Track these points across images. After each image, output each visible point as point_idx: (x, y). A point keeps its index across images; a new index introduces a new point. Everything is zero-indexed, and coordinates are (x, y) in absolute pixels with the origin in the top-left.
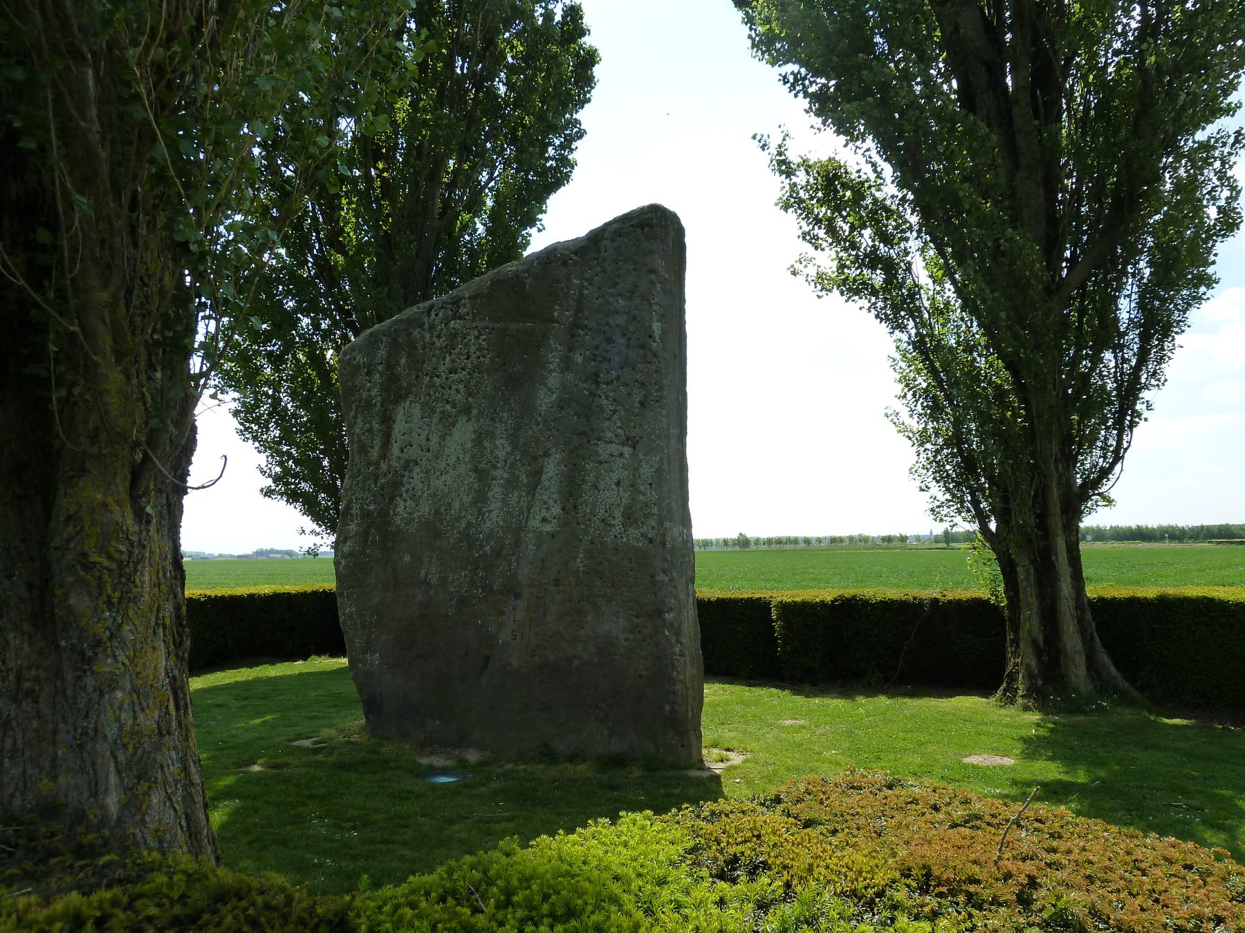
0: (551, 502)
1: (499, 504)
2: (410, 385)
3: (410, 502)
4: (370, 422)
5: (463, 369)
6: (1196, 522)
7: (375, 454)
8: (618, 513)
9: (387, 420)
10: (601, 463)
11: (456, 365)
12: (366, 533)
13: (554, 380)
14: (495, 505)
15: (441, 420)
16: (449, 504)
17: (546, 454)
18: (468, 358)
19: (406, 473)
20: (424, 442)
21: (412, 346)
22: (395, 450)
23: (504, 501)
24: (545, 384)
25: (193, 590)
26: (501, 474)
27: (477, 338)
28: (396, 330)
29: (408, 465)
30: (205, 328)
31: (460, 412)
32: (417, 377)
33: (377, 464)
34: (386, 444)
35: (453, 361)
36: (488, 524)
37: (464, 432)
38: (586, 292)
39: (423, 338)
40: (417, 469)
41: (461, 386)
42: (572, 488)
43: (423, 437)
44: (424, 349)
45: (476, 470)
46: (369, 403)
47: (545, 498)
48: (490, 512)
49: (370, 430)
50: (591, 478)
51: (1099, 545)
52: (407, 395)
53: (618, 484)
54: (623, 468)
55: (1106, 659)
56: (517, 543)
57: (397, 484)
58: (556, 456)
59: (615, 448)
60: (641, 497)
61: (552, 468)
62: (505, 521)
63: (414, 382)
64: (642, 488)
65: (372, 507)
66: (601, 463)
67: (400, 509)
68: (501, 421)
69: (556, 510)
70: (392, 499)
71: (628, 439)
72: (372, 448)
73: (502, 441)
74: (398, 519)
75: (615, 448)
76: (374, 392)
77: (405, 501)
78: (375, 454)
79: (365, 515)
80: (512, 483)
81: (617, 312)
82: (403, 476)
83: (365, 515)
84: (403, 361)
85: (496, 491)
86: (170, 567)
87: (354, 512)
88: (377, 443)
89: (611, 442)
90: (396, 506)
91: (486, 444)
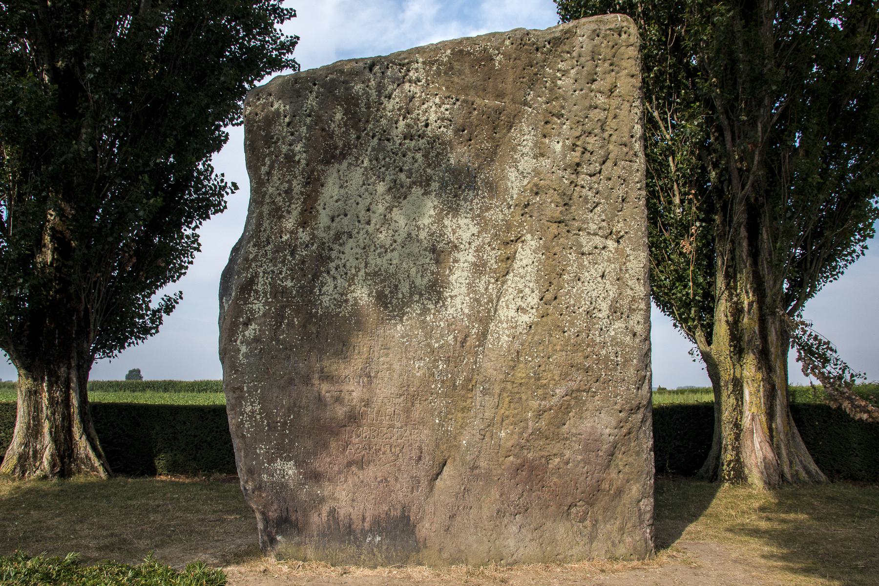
1: (464, 289)
2: (347, 145)
3: (340, 281)
8: (605, 306)
9: (314, 183)
10: (583, 254)
11: (413, 131)
12: (279, 316)
13: (527, 164)
15: (390, 189)
16: (396, 286)
19: (336, 247)
22: (324, 219)
23: (470, 286)
24: (516, 167)
28: (332, 80)
30: (797, 134)
31: (414, 183)
36: (451, 311)
38: (559, 82)
40: (351, 243)
41: (419, 156)
42: (551, 279)
43: (362, 207)
44: (368, 108)
46: (290, 158)
49: (289, 192)
50: (573, 268)
52: (343, 156)
54: (609, 261)
55: (765, 236)
57: (322, 259)
58: (532, 242)
60: (629, 292)
61: (527, 256)
62: (472, 308)
64: (630, 283)
65: (289, 284)
66: (583, 254)
67: (329, 288)
69: (533, 300)
70: (316, 276)
72: (289, 212)
74: (326, 299)
75: (598, 241)
76: (298, 148)
77: (335, 278)
79: (277, 292)
80: (479, 268)
83: (277, 292)
84: (338, 116)
87: (260, 287)
88: (296, 208)
89: (595, 234)
90: (323, 284)
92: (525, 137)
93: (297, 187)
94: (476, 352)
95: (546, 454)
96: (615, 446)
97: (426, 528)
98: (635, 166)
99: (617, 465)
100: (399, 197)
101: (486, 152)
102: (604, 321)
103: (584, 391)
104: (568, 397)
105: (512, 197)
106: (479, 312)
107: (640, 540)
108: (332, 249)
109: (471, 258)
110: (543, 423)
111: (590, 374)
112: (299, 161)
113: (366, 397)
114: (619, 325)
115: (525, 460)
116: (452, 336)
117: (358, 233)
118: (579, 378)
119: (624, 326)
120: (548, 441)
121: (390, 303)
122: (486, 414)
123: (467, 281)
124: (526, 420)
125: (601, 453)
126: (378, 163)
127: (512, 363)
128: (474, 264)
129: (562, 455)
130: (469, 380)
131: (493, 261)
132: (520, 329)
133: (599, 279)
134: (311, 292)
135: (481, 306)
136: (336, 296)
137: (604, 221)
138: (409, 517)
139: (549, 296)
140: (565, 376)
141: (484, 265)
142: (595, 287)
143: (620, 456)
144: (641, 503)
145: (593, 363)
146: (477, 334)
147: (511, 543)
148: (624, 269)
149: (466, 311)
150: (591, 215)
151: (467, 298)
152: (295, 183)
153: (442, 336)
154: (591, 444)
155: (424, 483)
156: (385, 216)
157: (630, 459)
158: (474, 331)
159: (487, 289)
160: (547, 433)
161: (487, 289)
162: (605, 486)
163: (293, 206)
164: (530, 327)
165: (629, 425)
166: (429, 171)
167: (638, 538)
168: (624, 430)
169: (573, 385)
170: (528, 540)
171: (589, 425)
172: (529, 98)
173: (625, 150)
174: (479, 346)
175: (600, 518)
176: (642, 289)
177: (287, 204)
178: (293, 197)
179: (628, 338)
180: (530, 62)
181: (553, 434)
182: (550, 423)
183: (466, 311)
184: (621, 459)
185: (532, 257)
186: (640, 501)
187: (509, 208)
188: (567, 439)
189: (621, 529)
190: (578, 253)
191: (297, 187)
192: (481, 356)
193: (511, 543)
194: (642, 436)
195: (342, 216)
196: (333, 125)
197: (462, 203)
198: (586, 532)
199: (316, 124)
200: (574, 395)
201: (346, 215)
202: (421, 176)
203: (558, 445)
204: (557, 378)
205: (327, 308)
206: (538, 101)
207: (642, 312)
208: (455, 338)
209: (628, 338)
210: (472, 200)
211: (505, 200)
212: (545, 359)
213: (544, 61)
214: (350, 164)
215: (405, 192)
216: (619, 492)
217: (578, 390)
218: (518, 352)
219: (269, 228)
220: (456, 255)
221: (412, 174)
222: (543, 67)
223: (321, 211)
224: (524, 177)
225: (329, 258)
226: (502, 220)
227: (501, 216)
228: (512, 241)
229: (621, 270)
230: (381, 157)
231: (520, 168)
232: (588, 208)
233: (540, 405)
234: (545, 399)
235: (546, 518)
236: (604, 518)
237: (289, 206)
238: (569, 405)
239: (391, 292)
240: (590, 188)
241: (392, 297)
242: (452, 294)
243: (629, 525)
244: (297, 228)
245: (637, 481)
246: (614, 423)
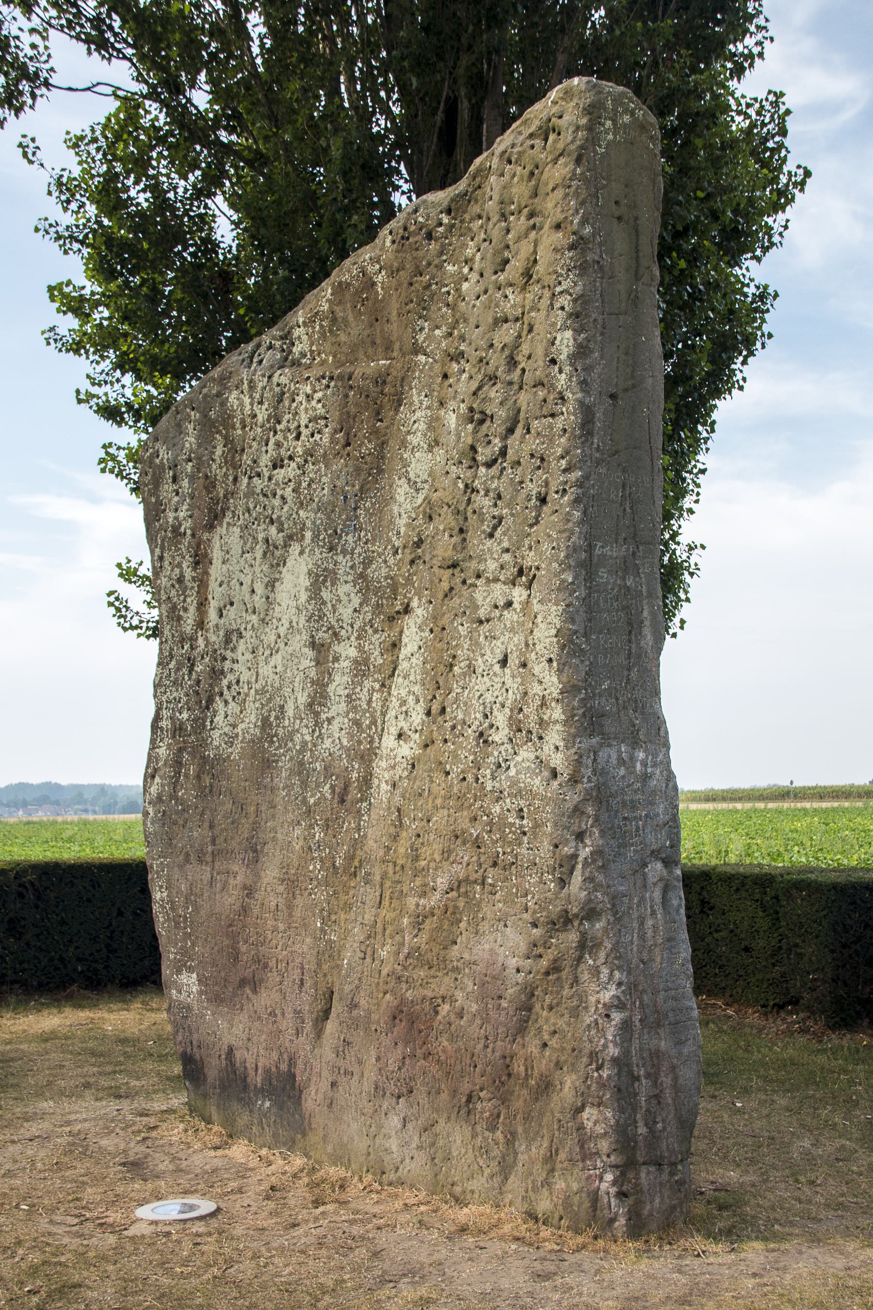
0: (411, 699)
4: (179, 565)
5: (291, 458)
6: (725, 787)
7: (190, 618)
8: (501, 718)
9: (201, 560)
10: (481, 622)
14: (337, 707)
17: (407, 610)
18: (298, 437)
19: (229, 654)
20: (248, 596)
21: (227, 420)
25: (704, 843)
26: (348, 651)
27: (309, 397)
29: (230, 637)
32: (235, 479)
33: (193, 639)
34: (202, 605)
35: (278, 445)
36: (328, 743)
37: (298, 570)
39: (241, 404)
42: (442, 671)
43: (246, 588)
45: (313, 645)
47: (403, 693)
48: (329, 721)
49: (180, 580)
51: (694, 806)
53: (504, 662)
54: (512, 630)
56: (366, 781)
59: (499, 592)
62: (351, 736)
63: (231, 488)
66: (481, 622)
67: (219, 719)
68: (344, 552)
69: (418, 717)
71: (521, 572)
72: (186, 610)
73: (348, 588)
75: (499, 592)
77: (226, 702)
78: (190, 618)
80: (361, 668)
81: (506, 321)
82: (224, 659)
85: (339, 685)
86: (216, 554)
88: (192, 602)
89: (496, 580)
91: (325, 595)
92: (416, 416)
93: (188, 573)
94: (359, 811)
95: (429, 994)
96: (529, 992)
97: (313, 1098)
98: (559, 423)
99: (540, 1030)
100: (278, 565)
101: (368, 459)
102: (502, 748)
103: (475, 882)
104: (454, 894)
105: (399, 533)
106: (360, 742)
107: (580, 1191)
108: (224, 659)
109: (353, 652)
110: (424, 936)
111: (482, 850)
112: (185, 534)
113: (249, 882)
114: (526, 754)
115: (403, 1001)
116: (328, 786)
117: (245, 629)
118: (466, 859)
119: (532, 756)
120: (432, 972)
121: (276, 735)
122: (366, 916)
123: (347, 691)
124: (403, 930)
125: (504, 1004)
126: (250, 515)
127: (392, 830)
128: (356, 662)
129: (453, 1000)
130: (350, 858)
131: (377, 653)
132: (399, 771)
133: (497, 668)
134: (204, 726)
135: (363, 732)
136: (226, 730)
137: (507, 550)
138: (294, 1076)
139: (435, 707)
140: (446, 853)
141: (366, 661)
142: (489, 684)
143: (545, 1013)
144: (585, 1115)
145: (483, 830)
146: (358, 780)
147: (393, 1144)
148: (530, 642)
149: (345, 742)
150: (489, 543)
151: (346, 720)
152: (185, 565)
153: (318, 785)
154: (489, 985)
155: (308, 1026)
156: (268, 598)
157: (561, 1023)
158: (355, 775)
159: (370, 702)
160: (429, 956)
161: (370, 702)
162: (519, 1068)
163: (189, 600)
164: (413, 766)
165: (550, 955)
166: (301, 512)
167: (575, 1186)
168: (544, 963)
169: (458, 870)
170: (414, 1145)
171: (487, 946)
172: (421, 338)
173: (541, 393)
174: (361, 800)
175: (520, 1130)
176: (555, 679)
177: (182, 598)
178: (186, 587)
179: (537, 781)
180: (417, 267)
181: (436, 959)
182: (432, 940)
183: (345, 742)
184: (547, 1020)
185: (418, 638)
186: (580, 1110)
187: (396, 552)
188: (456, 970)
189: (550, 1158)
190: (473, 622)
191: (188, 573)
192: (366, 818)
193: (393, 1144)
194: (585, 976)
195: (228, 607)
196: (214, 467)
197: (340, 558)
198: (496, 1152)
199: (199, 471)
200: (462, 890)
201: (232, 604)
202: (295, 523)
203: (446, 979)
204: (437, 857)
205: (217, 748)
206: (434, 337)
207: (558, 727)
208: (332, 787)
209: (537, 781)
210: (353, 549)
211: (389, 541)
212: (425, 823)
213: (441, 253)
214: (228, 524)
215: (282, 555)
216: (546, 1087)
217: (467, 880)
218: (399, 810)
219: (170, 637)
220: (336, 648)
221: (282, 525)
222: (440, 267)
223: (212, 601)
224: (417, 490)
225: (222, 672)
226: (386, 578)
227: (384, 571)
228: (398, 612)
229: (527, 645)
230: (251, 506)
231: (412, 475)
232: (484, 532)
233: (418, 905)
234: (424, 894)
235: (438, 1111)
236: (525, 1131)
237: (184, 601)
238: (456, 907)
239: (277, 718)
240: (487, 492)
241: (278, 726)
242: (330, 715)
243: (562, 1156)
244: (196, 633)
245: (573, 1069)
246: (523, 947)
